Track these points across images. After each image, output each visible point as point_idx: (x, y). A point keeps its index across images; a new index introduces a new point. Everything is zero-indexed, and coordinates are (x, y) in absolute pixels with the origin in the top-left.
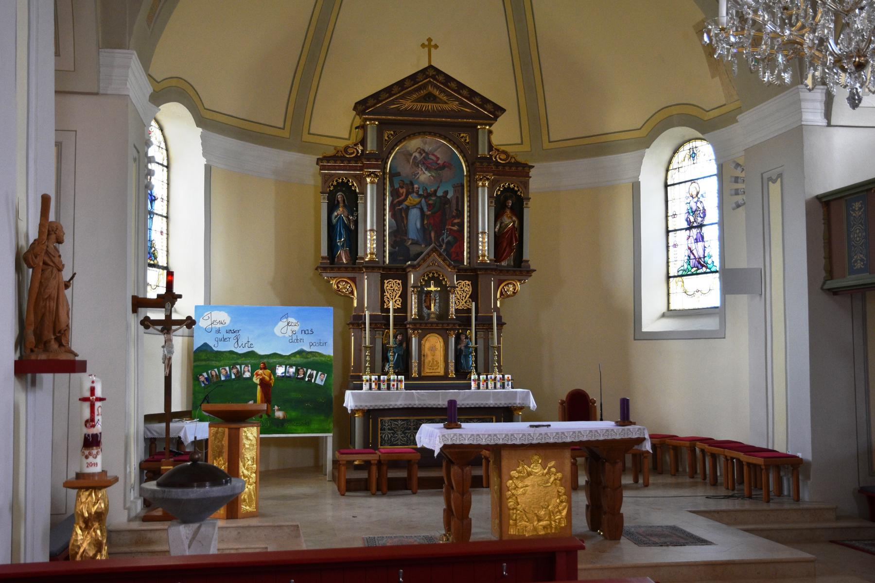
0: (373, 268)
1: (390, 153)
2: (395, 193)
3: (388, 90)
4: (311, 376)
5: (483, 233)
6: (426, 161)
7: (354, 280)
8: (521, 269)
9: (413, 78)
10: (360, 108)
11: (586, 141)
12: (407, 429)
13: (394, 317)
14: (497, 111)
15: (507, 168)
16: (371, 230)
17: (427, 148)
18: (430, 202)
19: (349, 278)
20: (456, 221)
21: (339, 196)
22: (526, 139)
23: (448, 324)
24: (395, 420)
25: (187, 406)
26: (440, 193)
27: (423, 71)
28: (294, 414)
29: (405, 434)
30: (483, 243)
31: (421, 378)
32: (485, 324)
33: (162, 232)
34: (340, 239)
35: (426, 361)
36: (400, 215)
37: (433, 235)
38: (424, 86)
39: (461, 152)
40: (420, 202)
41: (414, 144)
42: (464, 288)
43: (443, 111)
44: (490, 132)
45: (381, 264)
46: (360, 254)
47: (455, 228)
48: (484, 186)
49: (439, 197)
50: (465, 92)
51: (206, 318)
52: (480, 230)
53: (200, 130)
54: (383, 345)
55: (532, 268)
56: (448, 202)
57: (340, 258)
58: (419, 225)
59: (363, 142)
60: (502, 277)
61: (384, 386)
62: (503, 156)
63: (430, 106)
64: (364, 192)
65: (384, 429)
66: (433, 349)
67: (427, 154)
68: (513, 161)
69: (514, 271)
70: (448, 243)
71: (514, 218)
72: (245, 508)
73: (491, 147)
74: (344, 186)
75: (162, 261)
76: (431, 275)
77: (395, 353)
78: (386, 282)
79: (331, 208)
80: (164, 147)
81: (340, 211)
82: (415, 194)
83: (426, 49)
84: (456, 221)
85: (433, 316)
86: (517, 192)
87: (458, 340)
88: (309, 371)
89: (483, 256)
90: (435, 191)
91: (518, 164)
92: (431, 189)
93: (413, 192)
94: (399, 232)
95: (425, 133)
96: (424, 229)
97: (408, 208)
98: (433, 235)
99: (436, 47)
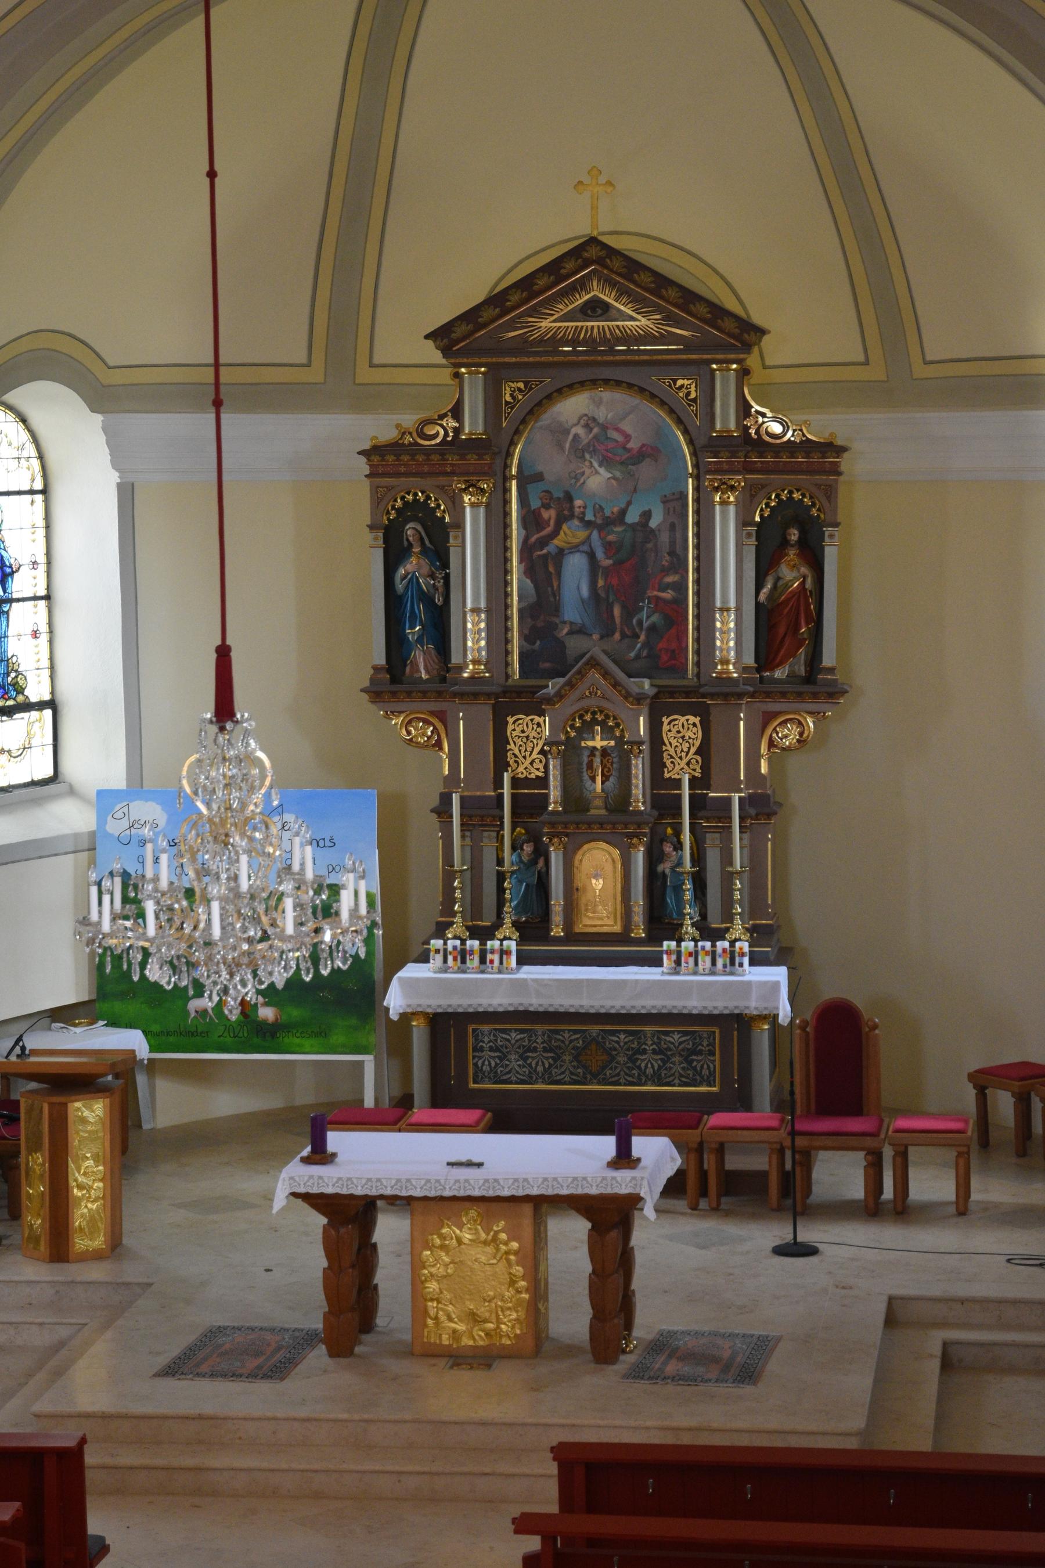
0: (476, 695)
3: (498, 301)
5: (725, 609)
6: (600, 444)
8: (818, 686)
11: (998, 368)
12: (529, 1050)
16: (475, 610)
17: (602, 414)
18: (611, 538)
19: (432, 713)
20: (670, 579)
21: (411, 530)
22: (876, 354)
24: (504, 1031)
25: (90, 994)
26: (632, 517)
28: (295, 1013)
31: (572, 937)
32: (762, 808)
33: (35, 634)
34: (412, 627)
36: (542, 567)
37: (617, 611)
38: (583, 285)
41: (572, 408)
46: (455, 659)
50: (515, 298)
51: (119, 815)
52: (718, 604)
53: (99, 417)
54: (818, 693)
56: (651, 534)
58: (585, 592)
59: (457, 412)
60: (772, 707)
61: (474, 962)
64: (459, 525)
65: (482, 1049)
67: (604, 428)
70: (653, 628)
71: (804, 570)
72: (81, 1243)
75: (37, 690)
76: (588, 717)
77: (520, 882)
78: (510, 720)
79: (394, 554)
80: (34, 453)
81: (413, 566)
82: (576, 522)
84: (670, 579)
87: (654, 858)
89: (725, 662)
92: (611, 509)
93: (572, 516)
94: (542, 608)
95: (594, 383)
96: (597, 600)
97: (561, 553)
98: (617, 611)
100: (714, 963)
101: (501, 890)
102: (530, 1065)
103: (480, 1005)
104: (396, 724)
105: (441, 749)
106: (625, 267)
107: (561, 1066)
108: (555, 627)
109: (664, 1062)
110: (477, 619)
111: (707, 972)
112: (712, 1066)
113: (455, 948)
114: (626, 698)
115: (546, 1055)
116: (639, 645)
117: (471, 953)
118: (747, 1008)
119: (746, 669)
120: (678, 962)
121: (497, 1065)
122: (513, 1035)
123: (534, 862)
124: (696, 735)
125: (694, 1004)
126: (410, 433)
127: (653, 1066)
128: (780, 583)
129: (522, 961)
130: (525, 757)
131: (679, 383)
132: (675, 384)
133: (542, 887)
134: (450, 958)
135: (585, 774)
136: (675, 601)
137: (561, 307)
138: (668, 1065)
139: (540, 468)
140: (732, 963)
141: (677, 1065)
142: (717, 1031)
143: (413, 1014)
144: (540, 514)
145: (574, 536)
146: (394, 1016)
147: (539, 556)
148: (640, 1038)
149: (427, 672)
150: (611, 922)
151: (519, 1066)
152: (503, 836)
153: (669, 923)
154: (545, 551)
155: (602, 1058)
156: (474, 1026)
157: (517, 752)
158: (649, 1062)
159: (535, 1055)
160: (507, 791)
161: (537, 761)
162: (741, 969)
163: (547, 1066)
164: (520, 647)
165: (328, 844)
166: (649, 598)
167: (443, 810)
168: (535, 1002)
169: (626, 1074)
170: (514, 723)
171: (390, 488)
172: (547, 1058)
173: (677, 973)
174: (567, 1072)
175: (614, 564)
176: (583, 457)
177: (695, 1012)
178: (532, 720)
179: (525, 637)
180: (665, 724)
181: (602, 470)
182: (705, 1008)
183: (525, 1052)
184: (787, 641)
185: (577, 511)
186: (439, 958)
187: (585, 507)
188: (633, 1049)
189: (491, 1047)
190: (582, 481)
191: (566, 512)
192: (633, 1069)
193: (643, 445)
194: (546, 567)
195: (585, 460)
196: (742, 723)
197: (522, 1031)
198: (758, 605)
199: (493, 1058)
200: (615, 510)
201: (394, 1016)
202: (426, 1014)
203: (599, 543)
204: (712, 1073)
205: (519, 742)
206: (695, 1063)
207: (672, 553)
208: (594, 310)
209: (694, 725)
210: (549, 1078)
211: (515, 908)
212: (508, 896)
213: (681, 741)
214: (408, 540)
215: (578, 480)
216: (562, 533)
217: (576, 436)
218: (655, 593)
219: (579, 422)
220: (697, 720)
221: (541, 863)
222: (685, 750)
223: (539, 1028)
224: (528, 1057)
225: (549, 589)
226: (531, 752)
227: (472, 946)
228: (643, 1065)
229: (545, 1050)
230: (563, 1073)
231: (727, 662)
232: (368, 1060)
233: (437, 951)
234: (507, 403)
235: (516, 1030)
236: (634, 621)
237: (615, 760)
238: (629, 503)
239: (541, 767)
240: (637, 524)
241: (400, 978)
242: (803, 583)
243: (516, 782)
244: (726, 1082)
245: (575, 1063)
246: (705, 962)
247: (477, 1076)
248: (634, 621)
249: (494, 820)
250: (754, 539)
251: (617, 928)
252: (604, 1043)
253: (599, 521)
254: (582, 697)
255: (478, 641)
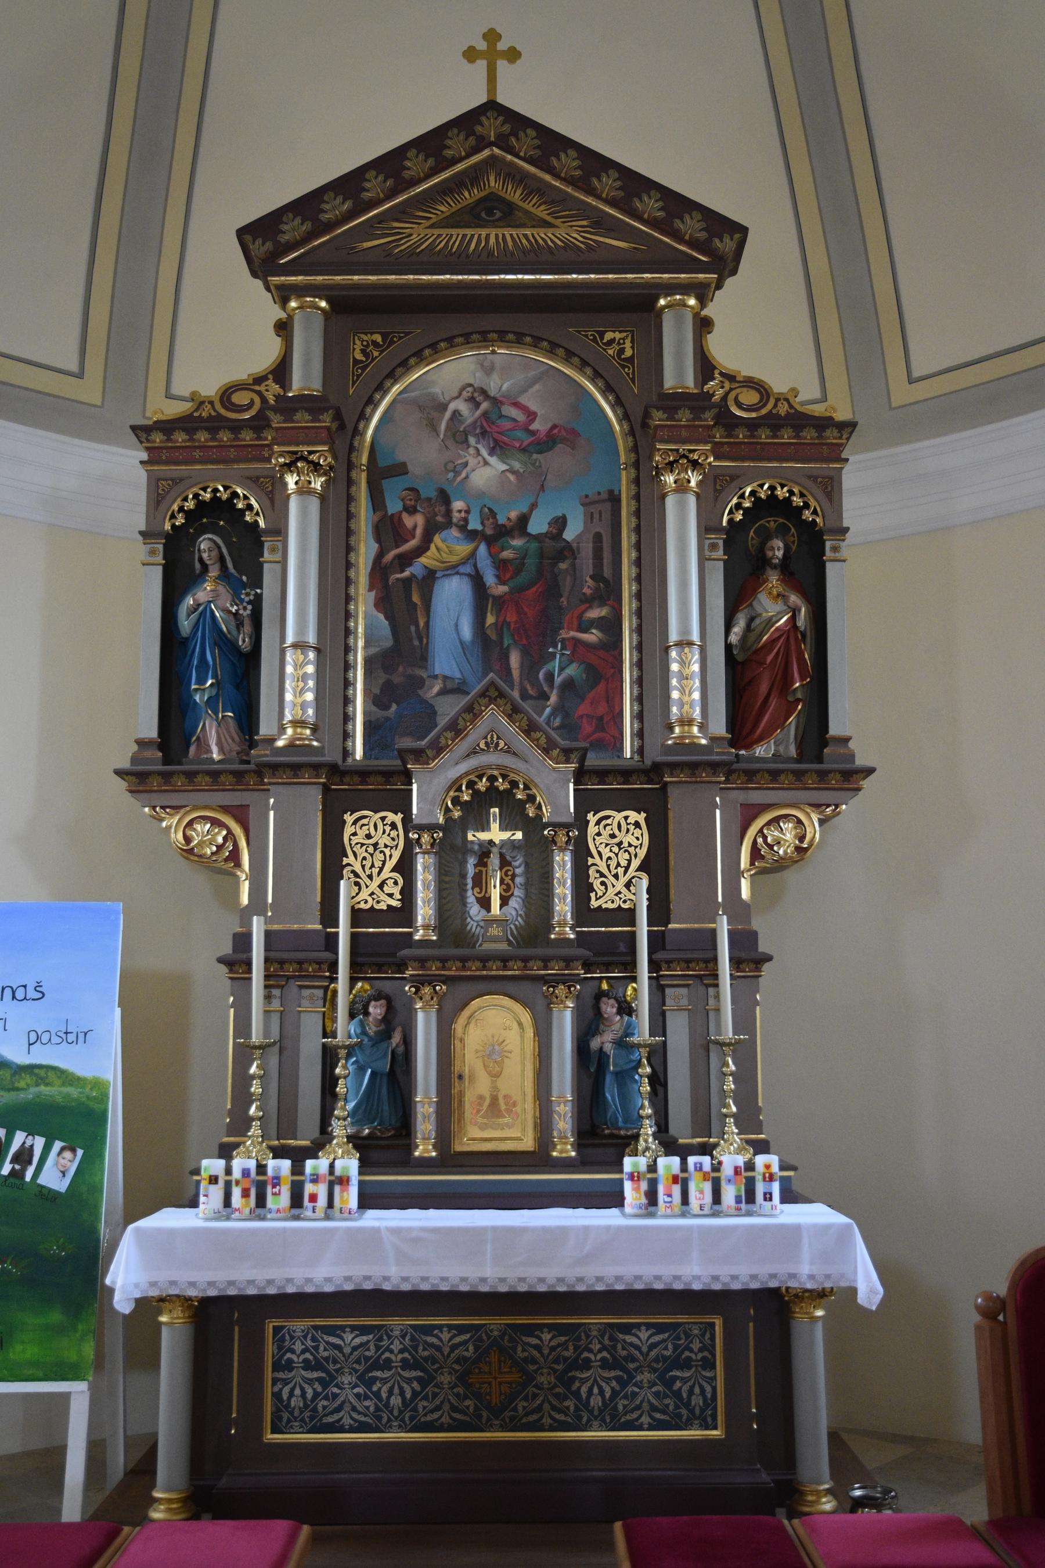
0: (296, 768)
1: (372, 402)
2: (389, 530)
3: (349, 185)
4: (24, 1157)
6: (491, 425)
7: (240, 814)
9: (431, 144)
10: (260, 248)
12: (377, 1365)
13: (355, 939)
14: (715, 244)
15: (764, 436)
17: (496, 385)
18: (507, 554)
19: (226, 809)
20: (595, 613)
23: (546, 962)
26: (538, 525)
27: (467, 122)
29: (369, 1383)
30: (683, 677)
31: (448, 1159)
34: (201, 681)
35: (469, 1097)
36: (404, 599)
37: (515, 660)
39: (608, 389)
40: (473, 555)
41: (451, 373)
42: (619, 838)
43: (536, 249)
44: (704, 325)
45: (333, 756)
46: (265, 729)
47: (593, 636)
48: (682, 487)
49: (537, 538)
52: (673, 637)
55: (860, 761)
56: (568, 551)
57: (203, 745)
58: (467, 631)
60: (756, 797)
61: (279, 1200)
62: (750, 397)
63: (492, 236)
64: (279, 531)
65: (289, 1366)
66: (494, 1056)
67: (496, 402)
68: (783, 409)
69: (799, 774)
70: (569, 685)
71: (794, 599)
73: (706, 367)
74: (217, 513)
76: (482, 785)
77: (361, 1069)
78: (349, 818)
79: (177, 580)
81: (206, 592)
82: (454, 532)
83: (482, 64)
84: (595, 613)
85: (495, 931)
86: (799, 510)
87: (589, 1025)
88: (19, 1138)
90: (523, 520)
91: (799, 420)
92: (508, 515)
93: (449, 524)
94: (400, 662)
95: (485, 338)
96: (487, 647)
97: (431, 576)
98: (515, 660)
99: (513, 55)
100: (717, 1198)
101: (329, 1082)
102: (377, 1395)
103: (289, 1281)
104: (169, 827)
105: (238, 865)
106: (538, 147)
107: (435, 1395)
108: (421, 683)
109: (623, 1383)
110: (301, 658)
111: (707, 1211)
112: (708, 1389)
113: (246, 1173)
114: (546, 751)
115: (407, 1374)
116: (548, 710)
117: (277, 1181)
118: (792, 1276)
119: (713, 739)
120: (652, 1197)
121: (316, 1395)
122: (348, 1337)
123: (385, 1034)
124: (639, 840)
125: (695, 1272)
126: (211, 403)
127: (602, 1392)
128: (757, 621)
129: (368, 1200)
130: (370, 877)
131: (609, 336)
132: (602, 338)
133: (395, 1081)
134: (236, 1192)
135: (469, 893)
136: (602, 646)
137: (443, 208)
138: (631, 1389)
139: (401, 457)
140: (751, 1198)
141: (646, 1388)
142: (718, 1322)
143: (162, 1300)
144: (400, 519)
145: (451, 552)
146: (122, 1303)
147: (398, 579)
148: (579, 1339)
149: (221, 750)
150: (516, 1134)
151: (358, 1396)
152: (335, 992)
153: (612, 1136)
154: (406, 574)
155: (508, 1378)
156: (277, 1323)
157: (358, 868)
158: (596, 1385)
159: (387, 1374)
160: (343, 930)
161: (390, 882)
162: (768, 1204)
163: (608, 1395)
164: (365, 713)
165: (32, 993)
166: (563, 641)
167: (237, 963)
168: (393, 1273)
169: (554, 1408)
170: (355, 823)
171: (176, 481)
172: (409, 1381)
173: (652, 1215)
174: (446, 1407)
175: (511, 592)
176: (466, 441)
177: (696, 1286)
178: (383, 819)
179: (377, 699)
180: (592, 824)
181: (493, 460)
182: (715, 1278)
183: (369, 1369)
184: (773, 703)
185: (456, 516)
186: (216, 1193)
187: (468, 512)
188: (566, 1359)
189: (306, 1361)
190: (463, 475)
191: (439, 519)
192: (566, 1398)
193: (554, 427)
194: (409, 597)
195: (469, 446)
196: (718, 812)
197: (364, 1330)
198: (728, 647)
199: (310, 1382)
200: (513, 515)
201: (122, 1303)
202: (185, 1301)
203: (489, 562)
204: (710, 1403)
205: (361, 852)
206: (678, 1384)
207: (597, 577)
208: (490, 212)
209: (637, 825)
210: (412, 1419)
211: (353, 1113)
212: (340, 1089)
213: (616, 849)
214: (201, 560)
215: (457, 474)
216: (433, 546)
217: (456, 413)
218: (572, 634)
219: (460, 394)
220: (641, 817)
221: (397, 1038)
222: (624, 863)
223: (397, 1323)
224: (374, 1380)
225: (413, 628)
226: (381, 869)
227: (277, 1169)
228: (584, 1390)
229: (406, 1365)
230: (438, 1408)
231: (690, 722)
232: (78, 1391)
233: (213, 1180)
234: (356, 362)
235: (353, 1328)
236: (541, 675)
237: (518, 871)
238: (533, 506)
239: (396, 891)
240: (546, 535)
241: (138, 1229)
242: (793, 619)
243: (358, 916)
244: (735, 1420)
245: (460, 1390)
246: (700, 1192)
247: (280, 1418)
248: (541, 675)
249: (320, 970)
250: (721, 552)
251: (528, 1143)
252: (514, 1349)
253: (489, 532)
254: (474, 752)
255: (302, 692)
